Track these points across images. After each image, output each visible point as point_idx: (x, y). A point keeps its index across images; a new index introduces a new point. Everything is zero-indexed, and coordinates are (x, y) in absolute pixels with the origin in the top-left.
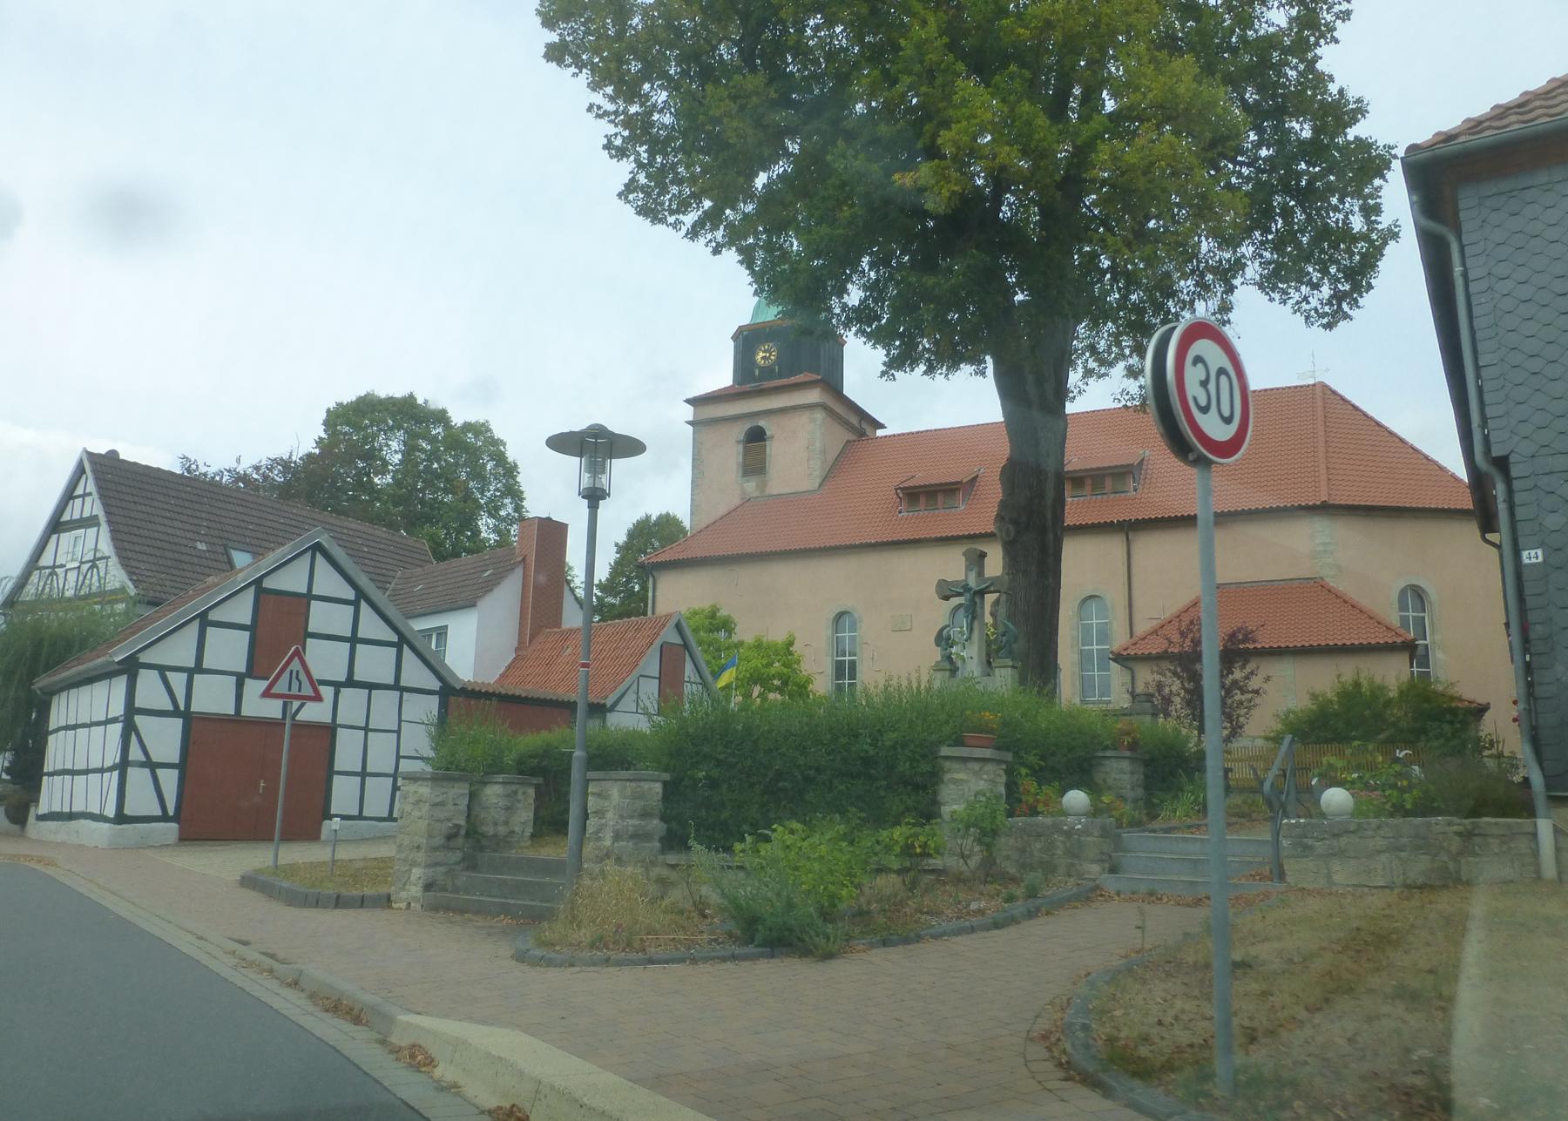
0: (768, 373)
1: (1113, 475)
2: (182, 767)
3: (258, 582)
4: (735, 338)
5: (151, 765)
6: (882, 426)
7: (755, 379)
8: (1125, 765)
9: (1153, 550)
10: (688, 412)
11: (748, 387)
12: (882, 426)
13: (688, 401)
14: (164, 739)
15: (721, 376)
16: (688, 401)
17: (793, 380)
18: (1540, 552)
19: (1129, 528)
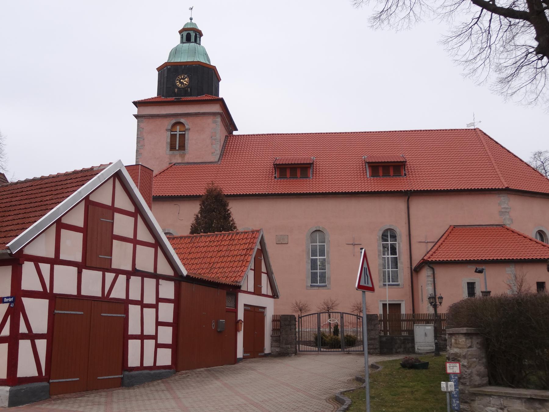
0: (184, 91)
1: (383, 166)
2: (49, 336)
3: (87, 198)
4: (160, 69)
5: (32, 337)
6: (236, 130)
7: (175, 95)
8: (462, 340)
9: (421, 208)
10: (135, 110)
11: (163, 99)
12: (236, 130)
13: (135, 103)
14: (37, 313)
15: (151, 91)
16: (135, 103)
17: (199, 98)
18: (133, 361)
19: (408, 195)
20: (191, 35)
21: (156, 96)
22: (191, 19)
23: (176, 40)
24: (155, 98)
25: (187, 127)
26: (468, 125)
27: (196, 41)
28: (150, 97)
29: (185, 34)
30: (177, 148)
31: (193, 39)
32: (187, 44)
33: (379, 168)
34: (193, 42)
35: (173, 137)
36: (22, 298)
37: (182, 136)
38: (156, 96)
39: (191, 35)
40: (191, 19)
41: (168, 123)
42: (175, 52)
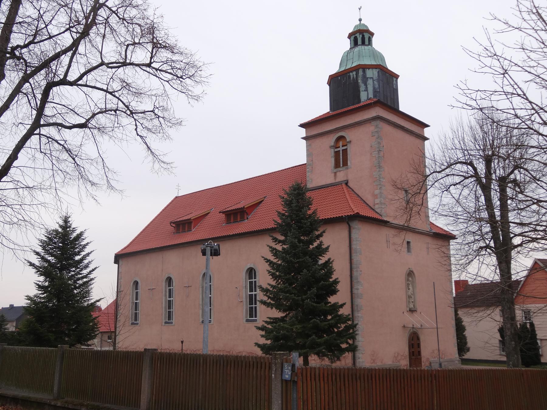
10: (303, 132)
13: (302, 126)
15: (323, 106)
16: (302, 126)
20: (361, 37)
21: (328, 110)
22: (360, 20)
23: (347, 45)
24: (328, 113)
25: (348, 140)
26: (332, 157)
27: (363, 43)
28: (318, 116)
29: (352, 38)
30: (341, 166)
31: (360, 42)
32: (363, 47)
33: (235, 215)
34: (360, 45)
35: (337, 154)
36: (341, 345)
37: (345, 152)
38: (328, 110)
39: (361, 37)
40: (360, 20)
41: (331, 140)
42: (346, 57)
